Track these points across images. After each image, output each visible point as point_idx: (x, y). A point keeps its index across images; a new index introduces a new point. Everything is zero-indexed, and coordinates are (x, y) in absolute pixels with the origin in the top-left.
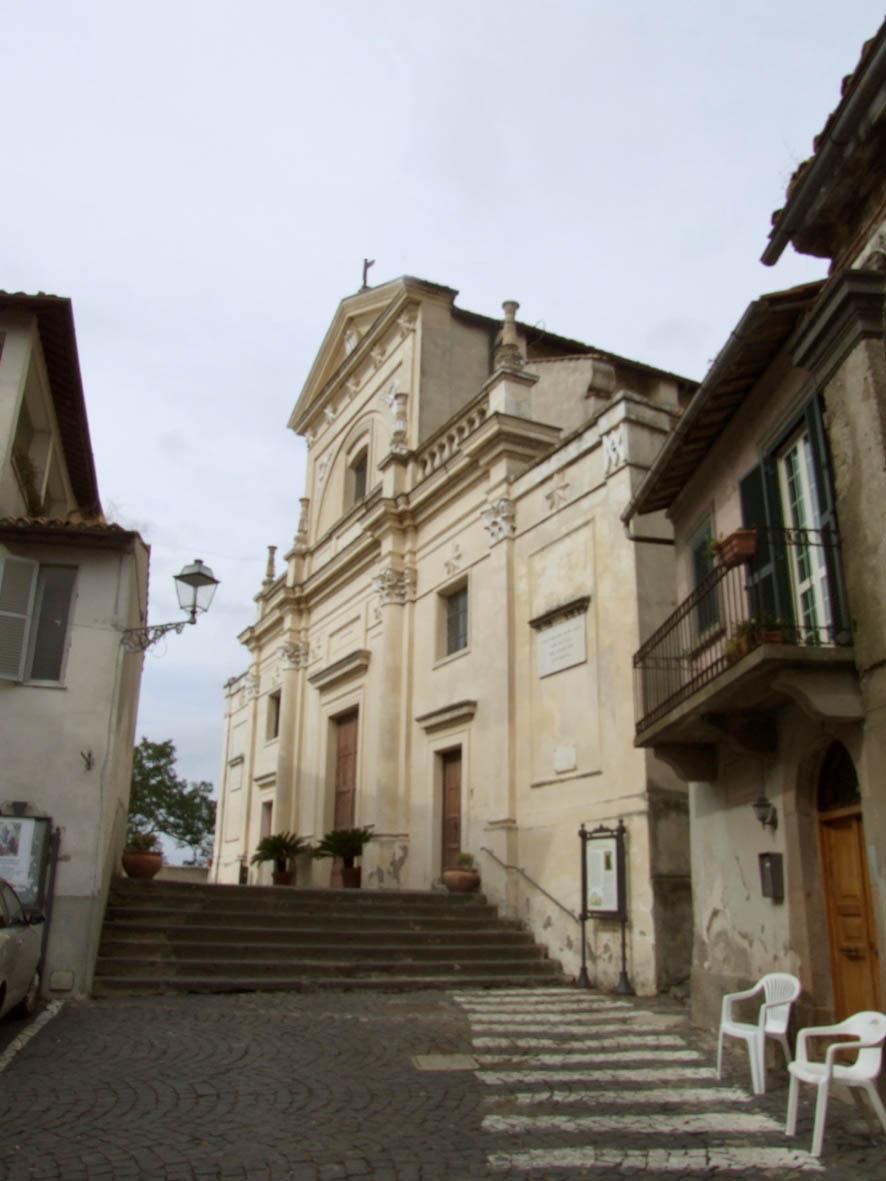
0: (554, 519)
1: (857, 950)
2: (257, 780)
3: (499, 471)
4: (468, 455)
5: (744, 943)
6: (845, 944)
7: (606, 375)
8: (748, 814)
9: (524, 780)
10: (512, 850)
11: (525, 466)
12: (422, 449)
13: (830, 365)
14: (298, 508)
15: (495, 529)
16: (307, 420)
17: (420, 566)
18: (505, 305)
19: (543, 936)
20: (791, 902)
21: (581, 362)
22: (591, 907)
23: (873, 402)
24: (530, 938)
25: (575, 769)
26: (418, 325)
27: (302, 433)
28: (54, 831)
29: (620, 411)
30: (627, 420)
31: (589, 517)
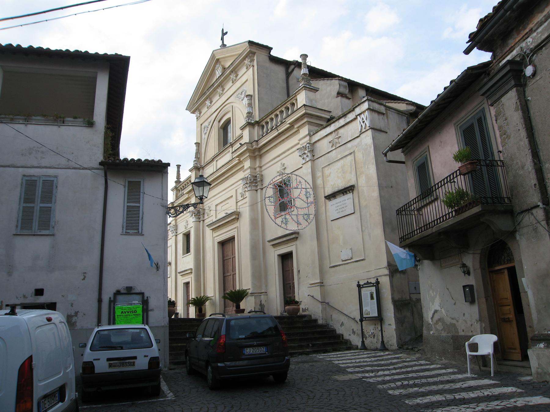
0: (334, 152)
1: (508, 318)
2: (179, 273)
3: (305, 131)
4: (289, 124)
5: (454, 322)
6: (502, 317)
7: (345, 87)
8: (457, 271)
9: (327, 264)
10: (323, 294)
11: (316, 128)
12: (262, 120)
13: (497, 96)
14: (194, 148)
15: (305, 156)
16: (196, 105)
17: (263, 173)
18: (301, 56)
19: (340, 330)
20: (478, 303)
21: (333, 81)
22: (364, 316)
23: (520, 112)
24: (334, 331)
25: (352, 259)
26: (255, 63)
27: (193, 112)
28: (146, 298)
29: (366, 106)
30: (369, 109)
31: (352, 151)
